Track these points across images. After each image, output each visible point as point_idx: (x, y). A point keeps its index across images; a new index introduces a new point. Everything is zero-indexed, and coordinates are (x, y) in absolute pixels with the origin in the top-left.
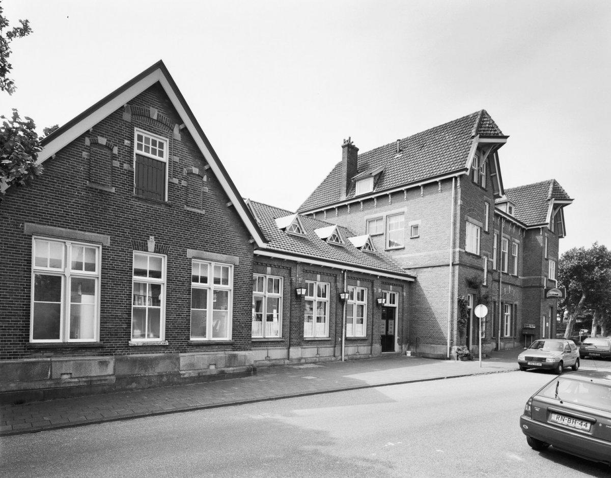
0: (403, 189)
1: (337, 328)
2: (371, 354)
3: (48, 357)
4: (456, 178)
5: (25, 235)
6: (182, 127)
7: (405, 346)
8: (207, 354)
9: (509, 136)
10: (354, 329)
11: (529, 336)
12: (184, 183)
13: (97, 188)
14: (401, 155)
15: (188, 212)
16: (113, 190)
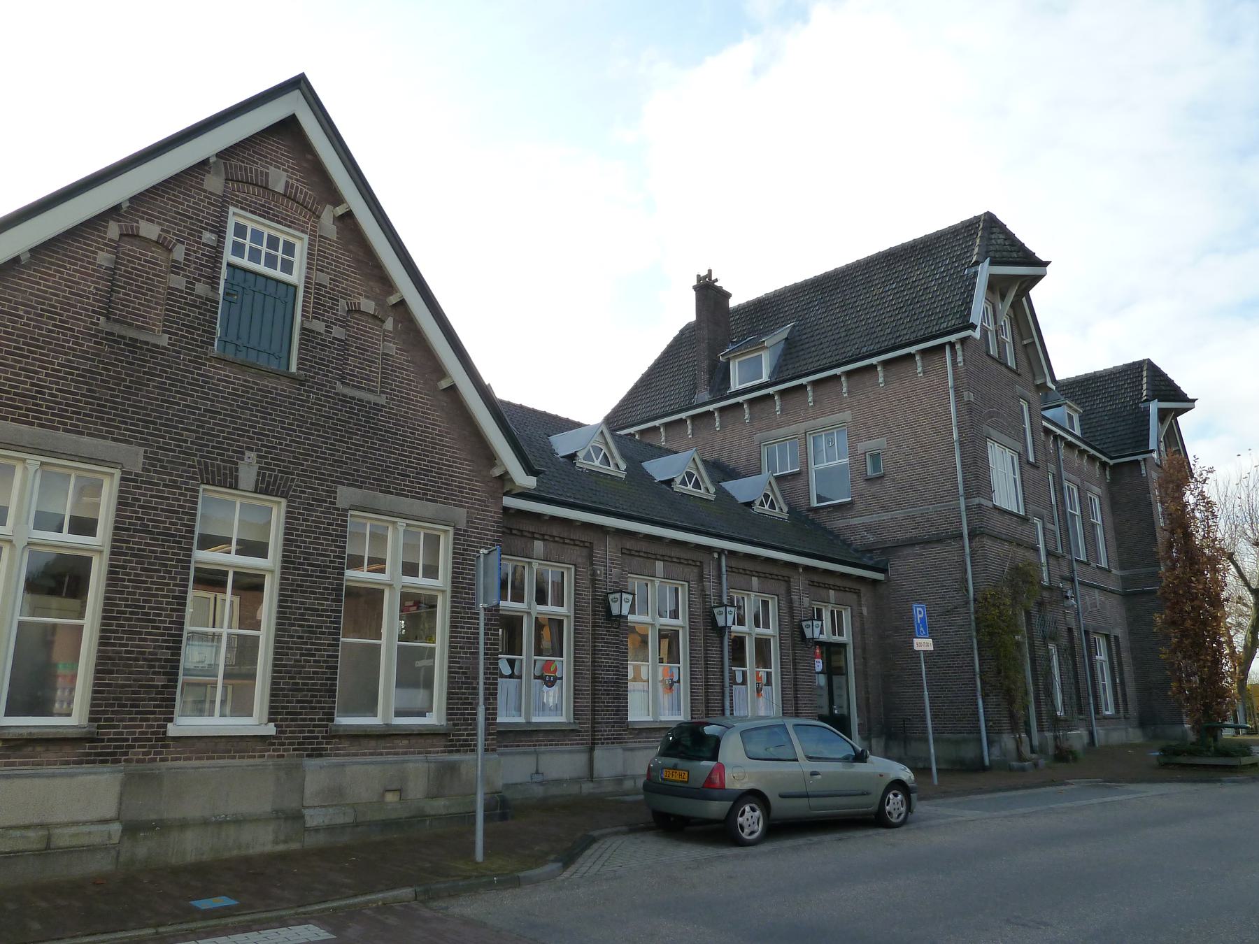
4: (952, 345)
13: (124, 333)
15: (345, 400)
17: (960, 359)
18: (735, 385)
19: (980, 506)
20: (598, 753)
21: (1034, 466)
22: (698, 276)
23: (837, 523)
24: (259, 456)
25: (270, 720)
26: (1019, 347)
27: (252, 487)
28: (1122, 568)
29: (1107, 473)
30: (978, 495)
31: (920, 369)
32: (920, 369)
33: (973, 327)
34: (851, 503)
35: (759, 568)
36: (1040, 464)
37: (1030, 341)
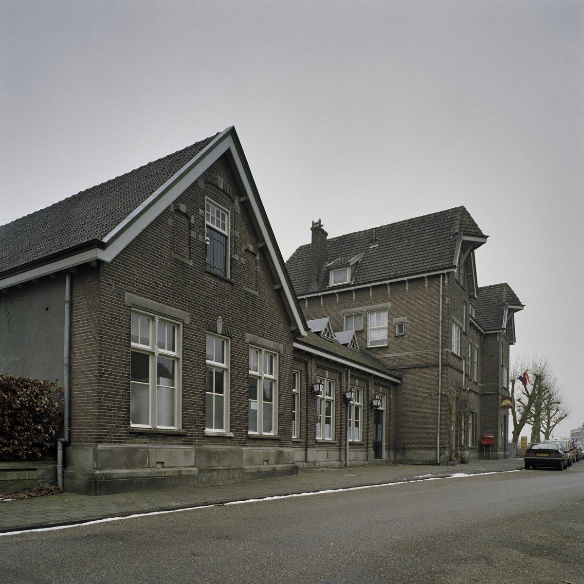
0: (387, 283)
1: (341, 432)
2: (367, 460)
3: (145, 443)
4: (444, 275)
5: (125, 306)
6: (242, 199)
7: (392, 453)
8: (261, 450)
9: (489, 236)
10: (355, 435)
11: (488, 446)
12: (243, 261)
13: (180, 259)
14: (377, 245)
15: (247, 293)
16: (191, 263)
17: (446, 282)
18: (332, 284)
19: (447, 352)
20: (309, 451)
21: (465, 334)
22: (313, 222)
23: (380, 356)
24: (222, 318)
25: (231, 431)
26: (466, 276)
27: (221, 333)
28: (482, 383)
29: (482, 338)
30: (447, 347)
31: (426, 285)
32: (426, 285)
33: (455, 267)
34: (387, 347)
35: (359, 376)
36: (467, 333)
37: (470, 274)
